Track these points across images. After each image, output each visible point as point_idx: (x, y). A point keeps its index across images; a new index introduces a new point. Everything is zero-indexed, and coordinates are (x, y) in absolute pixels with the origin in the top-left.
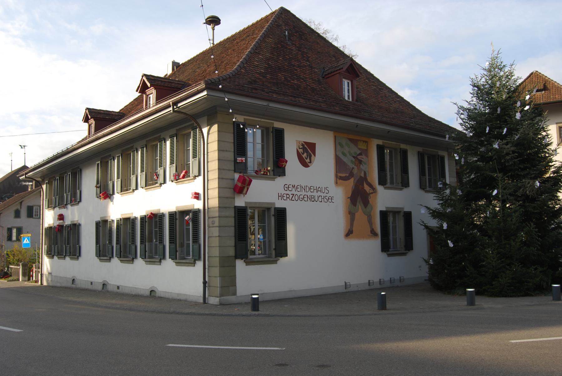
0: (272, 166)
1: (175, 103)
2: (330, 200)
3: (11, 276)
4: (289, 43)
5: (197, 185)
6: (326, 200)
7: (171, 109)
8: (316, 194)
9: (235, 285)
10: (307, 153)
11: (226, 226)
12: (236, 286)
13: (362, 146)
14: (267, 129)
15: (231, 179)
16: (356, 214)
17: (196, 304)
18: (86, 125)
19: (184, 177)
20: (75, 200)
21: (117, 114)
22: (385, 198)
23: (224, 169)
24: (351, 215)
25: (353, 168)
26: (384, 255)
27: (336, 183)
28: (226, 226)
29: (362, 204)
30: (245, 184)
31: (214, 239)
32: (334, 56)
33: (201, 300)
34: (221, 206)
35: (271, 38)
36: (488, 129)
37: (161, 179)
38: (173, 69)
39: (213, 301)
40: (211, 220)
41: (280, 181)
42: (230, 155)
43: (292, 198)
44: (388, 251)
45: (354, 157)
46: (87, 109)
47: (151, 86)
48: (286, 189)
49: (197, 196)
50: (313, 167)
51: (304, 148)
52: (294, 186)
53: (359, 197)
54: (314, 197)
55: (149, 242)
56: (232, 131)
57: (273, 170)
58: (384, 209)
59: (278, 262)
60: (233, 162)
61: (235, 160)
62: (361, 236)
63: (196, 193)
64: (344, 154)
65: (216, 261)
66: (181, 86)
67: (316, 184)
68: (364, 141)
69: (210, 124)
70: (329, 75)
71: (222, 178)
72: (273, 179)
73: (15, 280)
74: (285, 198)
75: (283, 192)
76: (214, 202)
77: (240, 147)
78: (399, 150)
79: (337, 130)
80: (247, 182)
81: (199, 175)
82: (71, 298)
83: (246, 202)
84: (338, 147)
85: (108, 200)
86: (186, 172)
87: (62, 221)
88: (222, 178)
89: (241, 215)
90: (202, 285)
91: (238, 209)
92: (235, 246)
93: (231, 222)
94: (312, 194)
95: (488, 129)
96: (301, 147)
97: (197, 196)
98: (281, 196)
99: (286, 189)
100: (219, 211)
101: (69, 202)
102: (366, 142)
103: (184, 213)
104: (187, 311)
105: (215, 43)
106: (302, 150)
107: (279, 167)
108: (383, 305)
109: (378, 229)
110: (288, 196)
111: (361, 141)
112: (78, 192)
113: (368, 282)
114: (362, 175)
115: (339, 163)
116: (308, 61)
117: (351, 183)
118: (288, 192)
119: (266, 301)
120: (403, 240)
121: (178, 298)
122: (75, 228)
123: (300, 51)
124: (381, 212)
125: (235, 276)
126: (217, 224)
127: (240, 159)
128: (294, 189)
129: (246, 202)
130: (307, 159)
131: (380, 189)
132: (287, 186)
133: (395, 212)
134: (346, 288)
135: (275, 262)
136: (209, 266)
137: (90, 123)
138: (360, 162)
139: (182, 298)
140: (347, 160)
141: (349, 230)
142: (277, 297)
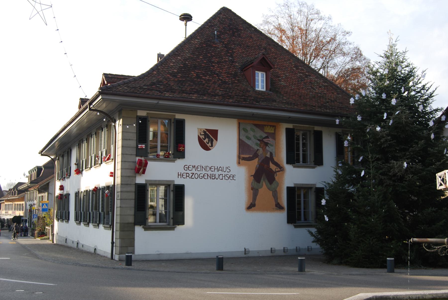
0: (173, 151)
2: (231, 178)
3: (46, 235)
4: (216, 41)
5: (108, 167)
6: (227, 178)
7: (88, 109)
8: (216, 173)
9: (133, 246)
10: (208, 139)
11: (126, 199)
12: (134, 246)
13: (269, 130)
15: (133, 162)
16: (260, 190)
22: (293, 176)
23: (127, 154)
24: (254, 192)
25: (258, 150)
26: (291, 226)
27: (239, 163)
28: (126, 199)
29: (267, 181)
30: (141, 166)
31: (121, 209)
32: (265, 48)
33: (109, 256)
34: (123, 183)
35: (199, 39)
39: (116, 257)
41: (180, 163)
42: (133, 143)
44: (295, 223)
45: (259, 140)
48: (186, 169)
50: (213, 150)
52: (194, 167)
53: (264, 174)
54: (215, 175)
57: (173, 154)
58: (292, 185)
59: (175, 229)
60: (135, 149)
64: (248, 138)
68: (271, 126)
70: (246, 68)
71: (125, 161)
72: (174, 161)
73: (47, 239)
76: (118, 180)
77: (142, 135)
78: (312, 132)
79: (241, 118)
80: (143, 165)
82: (354, 273)
83: (146, 180)
84: (242, 132)
85: (80, 175)
87: (62, 191)
88: (125, 161)
90: (111, 245)
91: (138, 186)
92: (135, 215)
93: (132, 196)
94: (212, 173)
98: (180, 175)
99: (186, 169)
100: (121, 187)
102: (273, 126)
103: (108, 187)
104: (152, 269)
105: (187, 37)
106: (203, 136)
107: (179, 153)
110: (188, 175)
111: (268, 126)
113: (270, 249)
114: (268, 155)
115: (243, 147)
116: (231, 56)
117: (255, 163)
118: (188, 172)
119: (149, 260)
122: (68, 195)
123: (225, 47)
124: (288, 188)
126: (119, 198)
127: (141, 145)
129: (146, 180)
130: (208, 143)
131: (289, 168)
132: (187, 167)
133: (307, 189)
134: (245, 254)
135: (173, 229)
136: (116, 231)
138: (266, 144)
140: (253, 143)
141: (251, 204)
142: (173, 258)
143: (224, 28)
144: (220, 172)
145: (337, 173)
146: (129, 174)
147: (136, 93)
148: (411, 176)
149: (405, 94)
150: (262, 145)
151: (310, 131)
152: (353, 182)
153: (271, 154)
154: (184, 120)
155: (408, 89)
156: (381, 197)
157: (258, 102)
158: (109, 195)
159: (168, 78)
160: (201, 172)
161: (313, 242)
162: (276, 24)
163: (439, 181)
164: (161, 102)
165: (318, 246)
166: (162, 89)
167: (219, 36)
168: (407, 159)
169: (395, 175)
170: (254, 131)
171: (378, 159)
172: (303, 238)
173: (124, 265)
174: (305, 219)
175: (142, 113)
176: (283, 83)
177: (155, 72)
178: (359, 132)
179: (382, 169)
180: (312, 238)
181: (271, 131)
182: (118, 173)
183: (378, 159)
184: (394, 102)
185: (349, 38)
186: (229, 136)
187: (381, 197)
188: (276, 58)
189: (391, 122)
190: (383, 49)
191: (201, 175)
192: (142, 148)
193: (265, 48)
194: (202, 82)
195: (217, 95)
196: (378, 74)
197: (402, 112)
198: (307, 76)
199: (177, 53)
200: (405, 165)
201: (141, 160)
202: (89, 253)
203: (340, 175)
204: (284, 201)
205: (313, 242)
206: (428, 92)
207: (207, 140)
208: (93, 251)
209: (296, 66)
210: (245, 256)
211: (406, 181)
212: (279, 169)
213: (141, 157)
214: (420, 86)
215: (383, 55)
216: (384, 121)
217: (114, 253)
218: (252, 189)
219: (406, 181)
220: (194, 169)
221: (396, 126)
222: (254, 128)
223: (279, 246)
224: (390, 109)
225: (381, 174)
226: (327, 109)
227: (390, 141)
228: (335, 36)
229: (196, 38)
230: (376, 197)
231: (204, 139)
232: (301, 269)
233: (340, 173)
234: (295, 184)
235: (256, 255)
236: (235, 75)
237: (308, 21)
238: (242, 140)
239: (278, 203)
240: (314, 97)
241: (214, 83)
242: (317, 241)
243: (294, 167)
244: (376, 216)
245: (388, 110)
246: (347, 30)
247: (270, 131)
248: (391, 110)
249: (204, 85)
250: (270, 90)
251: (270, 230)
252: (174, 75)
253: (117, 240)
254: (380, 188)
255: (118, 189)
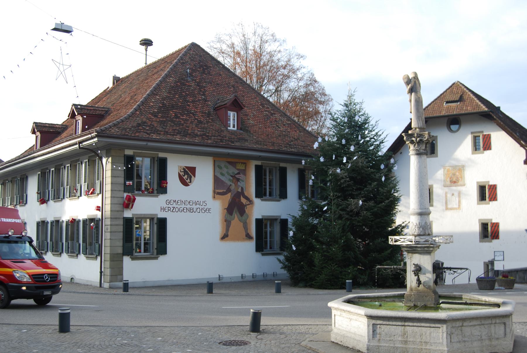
1: (80, 142)
2: (207, 211)
4: (189, 79)
5: (97, 200)
7: (77, 146)
8: (194, 207)
10: (187, 176)
13: (241, 167)
14: (154, 158)
16: (232, 222)
17: (95, 287)
18: (34, 135)
19: (92, 193)
20: (23, 202)
21: (60, 126)
22: (261, 209)
24: (227, 223)
25: (231, 185)
26: (259, 255)
29: (238, 213)
31: (109, 240)
32: (233, 86)
33: (99, 286)
35: (173, 78)
36: (334, 156)
37: (79, 194)
38: (114, 83)
39: (106, 285)
40: (106, 227)
41: (162, 198)
42: (121, 180)
43: (173, 210)
44: (263, 251)
45: (232, 176)
46: (35, 123)
47: (78, 114)
49: (98, 208)
50: (192, 186)
51: (185, 172)
52: (175, 201)
53: (236, 207)
55: (71, 240)
56: (123, 162)
58: (260, 217)
59: (159, 258)
61: (125, 183)
62: (236, 239)
63: (98, 207)
64: (222, 174)
65: (108, 257)
66: (104, 112)
67: (195, 199)
69: (108, 156)
72: (157, 196)
74: (167, 210)
75: (165, 206)
78: (278, 169)
80: (132, 200)
81: (100, 193)
84: (217, 169)
86: (94, 190)
89: (128, 223)
90: (99, 274)
92: (123, 246)
93: (121, 229)
95: (334, 156)
96: (182, 170)
97: (98, 208)
98: (163, 209)
101: (18, 203)
103: (92, 220)
105: (148, 63)
106: (183, 173)
107: (161, 187)
108: (210, 291)
109: (253, 233)
111: (239, 163)
112: (25, 194)
114: (240, 190)
116: (204, 95)
117: (228, 196)
118: (170, 206)
120: (279, 242)
121: (87, 284)
123: (198, 85)
125: (122, 267)
126: (109, 230)
128: (174, 204)
131: (257, 202)
133: (272, 220)
135: (156, 258)
137: (37, 135)
138: (238, 180)
139: (89, 284)
140: (226, 179)
142: (156, 285)
143: (195, 65)
144: (198, 206)
145: (303, 208)
146: (118, 209)
147: (127, 135)
148: (365, 212)
149: (361, 142)
150: (235, 180)
151: (276, 167)
152: (316, 215)
153: (242, 189)
154: (166, 158)
155: (364, 137)
156: (340, 230)
157: (233, 142)
158: (94, 227)
159: (151, 118)
160: (181, 206)
161: (282, 268)
162: (229, 43)
163: (390, 240)
164: (150, 144)
165: (286, 272)
166: (148, 130)
167: (191, 74)
168: (362, 197)
169: (352, 211)
170: (227, 168)
171: (338, 197)
172: (272, 264)
173: (121, 291)
174: (271, 248)
175: (129, 152)
176: (251, 122)
177: (138, 113)
178: (321, 172)
179: (341, 205)
180: (281, 265)
181: (242, 167)
182: (108, 208)
183: (338, 197)
184: (352, 148)
185: (303, 62)
186: (205, 172)
187: (340, 230)
188: (243, 96)
189: (350, 165)
190: (343, 99)
191: (181, 209)
192: (130, 185)
193: (233, 86)
194: (181, 121)
195: (197, 135)
196: (339, 120)
197: (358, 157)
198: (272, 114)
199: (155, 92)
200: (361, 203)
201: (130, 196)
202: (69, 283)
203: (305, 210)
204: (253, 232)
205: (282, 268)
206: (380, 138)
207: (186, 176)
208: (69, 280)
209: (262, 105)
210: (218, 282)
211: (361, 216)
212: (249, 203)
213: (129, 193)
214: (374, 133)
215: (343, 104)
216: (344, 164)
217: (102, 282)
218: (226, 221)
219: (361, 216)
220: (174, 204)
221: (353, 170)
222: (227, 164)
223: (248, 273)
224: (348, 154)
225: (341, 210)
226: (292, 148)
227: (348, 182)
228: (289, 60)
229: (171, 77)
230: (337, 230)
231: (184, 176)
232: (278, 291)
233: (306, 208)
234: (262, 216)
235: (229, 281)
236: (209, 114)
237: (263, 42)
238: (217, 177)
239: (248, 234)
240: (280, 136)
241: (192, 122)
242: (285, 267)
243: (262, 200)
244: (337, 246)
245: (347, 154)
246: (302, 53)
247: (241, 168)
248: (350, 156)
249: (183, 125)
250: (241, 129)
251: (241, 257)
252: (155, 115)
253: (106, 269)
254: (340, 221)
255: (107, 222)
